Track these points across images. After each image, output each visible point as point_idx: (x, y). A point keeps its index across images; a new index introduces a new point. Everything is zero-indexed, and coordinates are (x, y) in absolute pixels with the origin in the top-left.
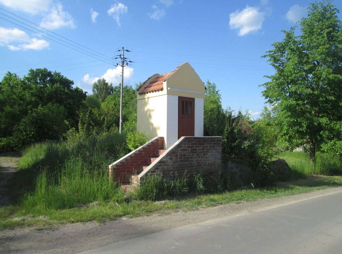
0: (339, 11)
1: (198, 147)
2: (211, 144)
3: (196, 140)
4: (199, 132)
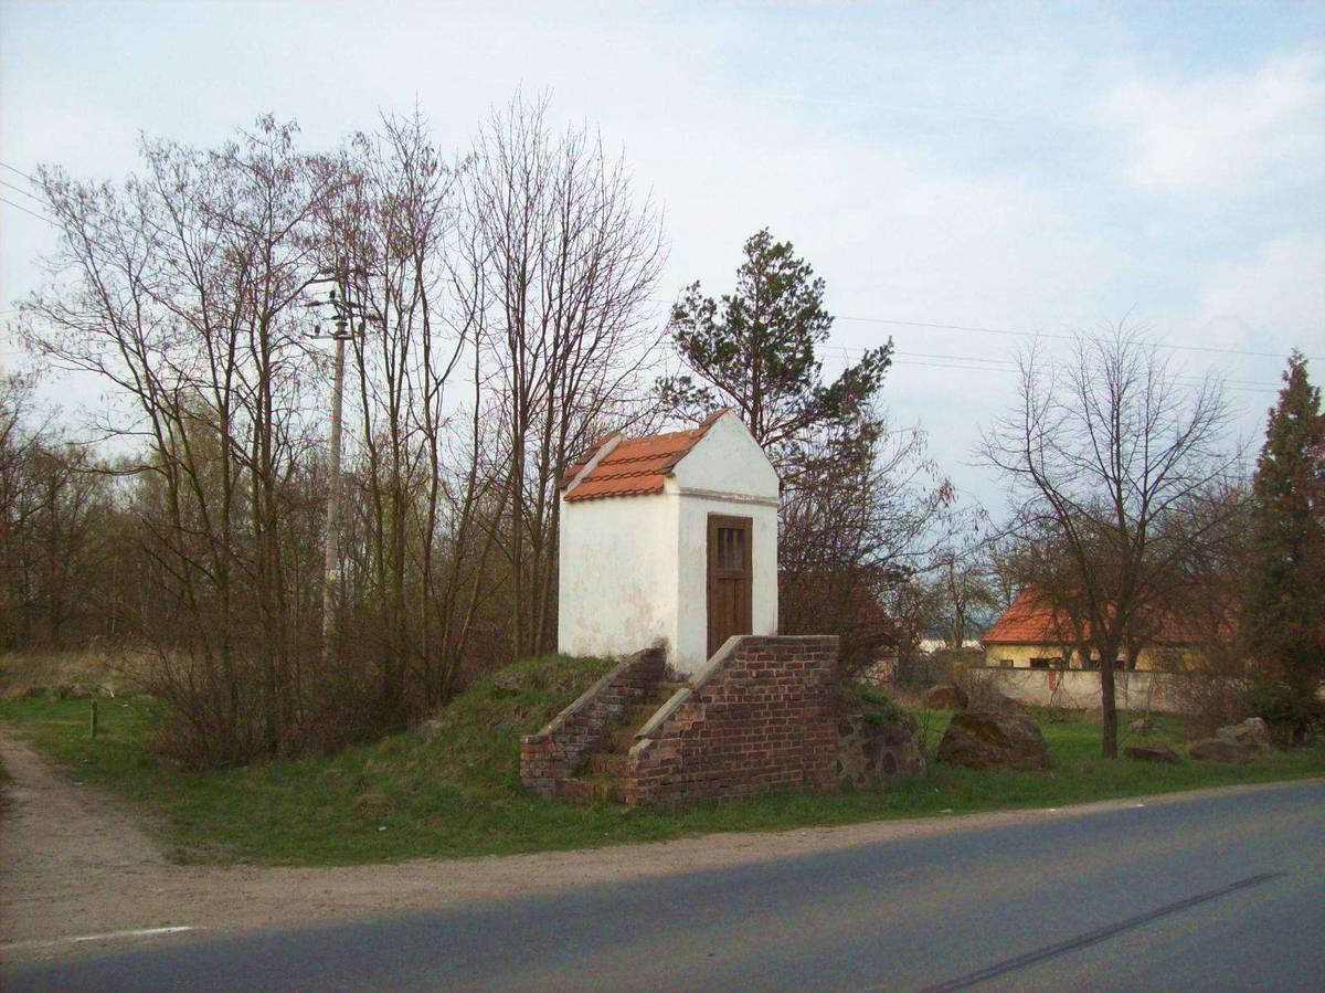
0: (830, 315)
1: (774, 666)
2: (810, 657)
3: (771, 645)
4: (765, 615)
